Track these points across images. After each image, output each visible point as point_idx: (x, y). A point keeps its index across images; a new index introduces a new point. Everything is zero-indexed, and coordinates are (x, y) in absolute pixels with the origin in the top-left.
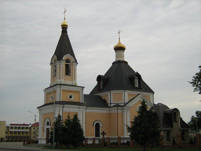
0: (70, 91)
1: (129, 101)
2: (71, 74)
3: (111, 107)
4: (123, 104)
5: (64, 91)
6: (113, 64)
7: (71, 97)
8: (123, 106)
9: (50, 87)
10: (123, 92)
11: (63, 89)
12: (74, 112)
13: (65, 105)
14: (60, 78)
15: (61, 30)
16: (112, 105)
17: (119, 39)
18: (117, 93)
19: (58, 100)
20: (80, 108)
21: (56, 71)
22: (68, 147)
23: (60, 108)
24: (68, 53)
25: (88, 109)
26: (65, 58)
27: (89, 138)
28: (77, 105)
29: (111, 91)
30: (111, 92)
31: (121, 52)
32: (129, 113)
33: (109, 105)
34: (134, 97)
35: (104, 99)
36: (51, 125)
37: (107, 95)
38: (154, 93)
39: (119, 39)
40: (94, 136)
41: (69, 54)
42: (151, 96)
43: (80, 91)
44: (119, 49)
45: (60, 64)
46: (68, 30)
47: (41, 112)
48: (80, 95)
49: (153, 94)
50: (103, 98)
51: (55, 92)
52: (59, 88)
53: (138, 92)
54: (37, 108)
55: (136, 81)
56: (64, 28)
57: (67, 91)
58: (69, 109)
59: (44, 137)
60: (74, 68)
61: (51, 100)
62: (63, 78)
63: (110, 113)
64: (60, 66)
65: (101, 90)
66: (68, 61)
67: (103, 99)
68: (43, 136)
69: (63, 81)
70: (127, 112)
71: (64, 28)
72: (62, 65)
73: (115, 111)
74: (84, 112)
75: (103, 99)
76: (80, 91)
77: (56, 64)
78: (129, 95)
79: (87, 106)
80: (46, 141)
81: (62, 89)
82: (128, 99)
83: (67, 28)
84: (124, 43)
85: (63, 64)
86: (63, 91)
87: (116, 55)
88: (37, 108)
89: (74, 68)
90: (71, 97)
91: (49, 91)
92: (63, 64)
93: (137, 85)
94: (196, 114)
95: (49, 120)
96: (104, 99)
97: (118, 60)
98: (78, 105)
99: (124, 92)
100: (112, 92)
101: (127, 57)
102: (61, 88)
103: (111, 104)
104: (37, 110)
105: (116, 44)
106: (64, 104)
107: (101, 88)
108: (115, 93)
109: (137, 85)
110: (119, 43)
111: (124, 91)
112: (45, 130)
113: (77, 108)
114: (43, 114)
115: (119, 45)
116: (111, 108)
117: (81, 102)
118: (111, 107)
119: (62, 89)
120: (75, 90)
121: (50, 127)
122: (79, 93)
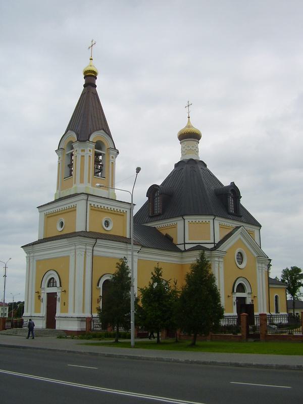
0: (110, 211)
1: (221, 238)
2: (105, 175)
3: (185, 251)
4: (212, 246)
5: (94, 209)
6: (176, 165)
7: (107, 223)
8: (212, 250)
9: (56, 201)
10: (211, 221)
11: (93, 205)
12: (114, 258)
13: (99, 241)
14: (82, 181)
15: (83, 82)
16: (188, 247)
17: (189, 117)
18: (194, 221)
19: (80, 227)
20: (127, 250)
21: (70, 166)
22: (117, 341)
23: (87, 247)
24: (100, 129)
25: (145, 253)
26: (93, 137)
27: (227, 316)
28: (123, 242)
29: (185, 217)
30: (184, 219)
31: (190, 143)
32: (222, 265)
33: (181, 247)
34: (229, 231)
35: (166, 234)
36: (61, 286)
37: (175, 227)
38: (260, 226)
39: (189, 117)
40: (232, 312)
41: (102, 131)
42: (256, 232)
43: (126, 211)
44: (190, 136)
45: (83, 151)
46: (97, 82)
47: (33, 256)
48: (125, 221)
49: (259, 228)
50: (164, 232)
51: (74, 209)
52: (84, 202)
53: (236, 222)
54: (22, 247)
55: (231, 201)
56: (90, 78)
57: (100, 209)
58: (106, 250)
59: (40, 312)
60: (112, 163)
61: (60, 229)
62: (89, 182)
63: (182, 265)
64: (83, 154)
65: (159, 215)
66: (99, 145)
67: (165, 235)
68: (37, 310)
69: (90, 187)
70: (219, 261)
71: (90, 78)
72: (89, 152)
73: (191, 259)
74: (136, 259)
75: (165, 235)
76: (126, 211)
77: (72, 151)
78: (221, 227)
79: (143, 246)
80: (45, 322)
81: (90, 204)
82: (220, 236)
83: (96, 78)
84: (197, 126)
85: (90, 150)
86: (93, 208)
87: (183, 148)
88: (22, 247)
89: (112, 163)
90: (107, 223)
91: (49, 211)
92: (90, 150)
93: (232, 210)
94: (286, 273)
95: (57, 273)
96: (166, 234)
97: (188, 157)
98: (125, 242)
99: (212, 220)
100: (188, 219)
101: (205, 150)
102: (89, 203)
103: (185, 244)
104: (23, 254)
105: (181, 126)
106: (96, 239)
107: (158, 210)
108: (194, 221)
109: (232, 210)
110: (189, 126)
111: (214, 219)
112: (44, 297)
113: (121, 249)
114: (37, 261)
115: (189, 130)
116: (185, 254)
117: (127, 237)
118: (185, 251)
119: (90, 204)
120: (112, 208)
121: (60, 291)
122: (123, 215)
